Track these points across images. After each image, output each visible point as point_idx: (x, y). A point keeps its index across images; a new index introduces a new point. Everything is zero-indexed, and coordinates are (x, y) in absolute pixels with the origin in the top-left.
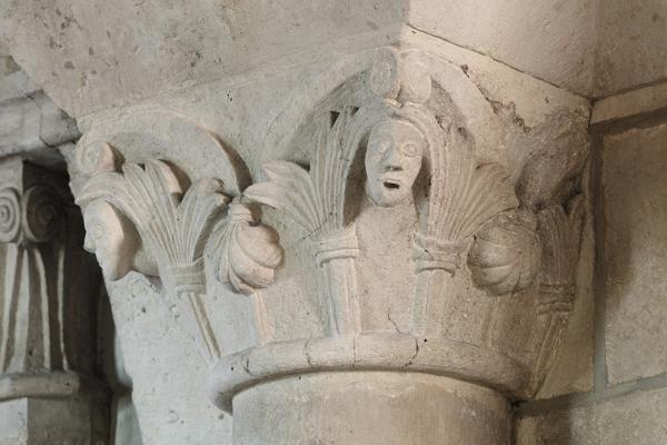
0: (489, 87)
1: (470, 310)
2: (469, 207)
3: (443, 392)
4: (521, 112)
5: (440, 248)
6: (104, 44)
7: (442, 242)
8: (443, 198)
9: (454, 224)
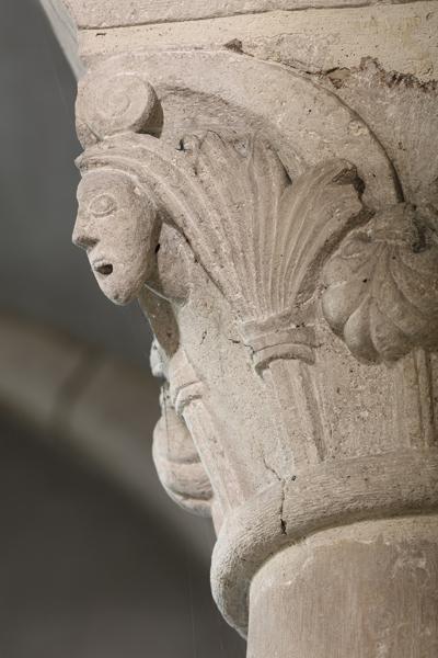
0: (301, 54)
1: (368, 403)
2: (286, 247)
3: (357, 548)
4: (394, 62)
5: (263, 328)
6: (145, 74)
7: (263, 319)
8: (234, 252)
9: (273, 284)
